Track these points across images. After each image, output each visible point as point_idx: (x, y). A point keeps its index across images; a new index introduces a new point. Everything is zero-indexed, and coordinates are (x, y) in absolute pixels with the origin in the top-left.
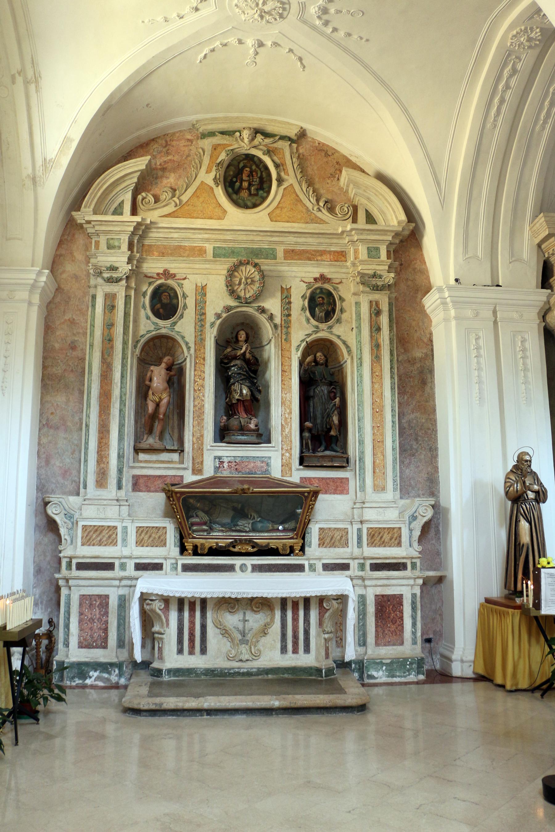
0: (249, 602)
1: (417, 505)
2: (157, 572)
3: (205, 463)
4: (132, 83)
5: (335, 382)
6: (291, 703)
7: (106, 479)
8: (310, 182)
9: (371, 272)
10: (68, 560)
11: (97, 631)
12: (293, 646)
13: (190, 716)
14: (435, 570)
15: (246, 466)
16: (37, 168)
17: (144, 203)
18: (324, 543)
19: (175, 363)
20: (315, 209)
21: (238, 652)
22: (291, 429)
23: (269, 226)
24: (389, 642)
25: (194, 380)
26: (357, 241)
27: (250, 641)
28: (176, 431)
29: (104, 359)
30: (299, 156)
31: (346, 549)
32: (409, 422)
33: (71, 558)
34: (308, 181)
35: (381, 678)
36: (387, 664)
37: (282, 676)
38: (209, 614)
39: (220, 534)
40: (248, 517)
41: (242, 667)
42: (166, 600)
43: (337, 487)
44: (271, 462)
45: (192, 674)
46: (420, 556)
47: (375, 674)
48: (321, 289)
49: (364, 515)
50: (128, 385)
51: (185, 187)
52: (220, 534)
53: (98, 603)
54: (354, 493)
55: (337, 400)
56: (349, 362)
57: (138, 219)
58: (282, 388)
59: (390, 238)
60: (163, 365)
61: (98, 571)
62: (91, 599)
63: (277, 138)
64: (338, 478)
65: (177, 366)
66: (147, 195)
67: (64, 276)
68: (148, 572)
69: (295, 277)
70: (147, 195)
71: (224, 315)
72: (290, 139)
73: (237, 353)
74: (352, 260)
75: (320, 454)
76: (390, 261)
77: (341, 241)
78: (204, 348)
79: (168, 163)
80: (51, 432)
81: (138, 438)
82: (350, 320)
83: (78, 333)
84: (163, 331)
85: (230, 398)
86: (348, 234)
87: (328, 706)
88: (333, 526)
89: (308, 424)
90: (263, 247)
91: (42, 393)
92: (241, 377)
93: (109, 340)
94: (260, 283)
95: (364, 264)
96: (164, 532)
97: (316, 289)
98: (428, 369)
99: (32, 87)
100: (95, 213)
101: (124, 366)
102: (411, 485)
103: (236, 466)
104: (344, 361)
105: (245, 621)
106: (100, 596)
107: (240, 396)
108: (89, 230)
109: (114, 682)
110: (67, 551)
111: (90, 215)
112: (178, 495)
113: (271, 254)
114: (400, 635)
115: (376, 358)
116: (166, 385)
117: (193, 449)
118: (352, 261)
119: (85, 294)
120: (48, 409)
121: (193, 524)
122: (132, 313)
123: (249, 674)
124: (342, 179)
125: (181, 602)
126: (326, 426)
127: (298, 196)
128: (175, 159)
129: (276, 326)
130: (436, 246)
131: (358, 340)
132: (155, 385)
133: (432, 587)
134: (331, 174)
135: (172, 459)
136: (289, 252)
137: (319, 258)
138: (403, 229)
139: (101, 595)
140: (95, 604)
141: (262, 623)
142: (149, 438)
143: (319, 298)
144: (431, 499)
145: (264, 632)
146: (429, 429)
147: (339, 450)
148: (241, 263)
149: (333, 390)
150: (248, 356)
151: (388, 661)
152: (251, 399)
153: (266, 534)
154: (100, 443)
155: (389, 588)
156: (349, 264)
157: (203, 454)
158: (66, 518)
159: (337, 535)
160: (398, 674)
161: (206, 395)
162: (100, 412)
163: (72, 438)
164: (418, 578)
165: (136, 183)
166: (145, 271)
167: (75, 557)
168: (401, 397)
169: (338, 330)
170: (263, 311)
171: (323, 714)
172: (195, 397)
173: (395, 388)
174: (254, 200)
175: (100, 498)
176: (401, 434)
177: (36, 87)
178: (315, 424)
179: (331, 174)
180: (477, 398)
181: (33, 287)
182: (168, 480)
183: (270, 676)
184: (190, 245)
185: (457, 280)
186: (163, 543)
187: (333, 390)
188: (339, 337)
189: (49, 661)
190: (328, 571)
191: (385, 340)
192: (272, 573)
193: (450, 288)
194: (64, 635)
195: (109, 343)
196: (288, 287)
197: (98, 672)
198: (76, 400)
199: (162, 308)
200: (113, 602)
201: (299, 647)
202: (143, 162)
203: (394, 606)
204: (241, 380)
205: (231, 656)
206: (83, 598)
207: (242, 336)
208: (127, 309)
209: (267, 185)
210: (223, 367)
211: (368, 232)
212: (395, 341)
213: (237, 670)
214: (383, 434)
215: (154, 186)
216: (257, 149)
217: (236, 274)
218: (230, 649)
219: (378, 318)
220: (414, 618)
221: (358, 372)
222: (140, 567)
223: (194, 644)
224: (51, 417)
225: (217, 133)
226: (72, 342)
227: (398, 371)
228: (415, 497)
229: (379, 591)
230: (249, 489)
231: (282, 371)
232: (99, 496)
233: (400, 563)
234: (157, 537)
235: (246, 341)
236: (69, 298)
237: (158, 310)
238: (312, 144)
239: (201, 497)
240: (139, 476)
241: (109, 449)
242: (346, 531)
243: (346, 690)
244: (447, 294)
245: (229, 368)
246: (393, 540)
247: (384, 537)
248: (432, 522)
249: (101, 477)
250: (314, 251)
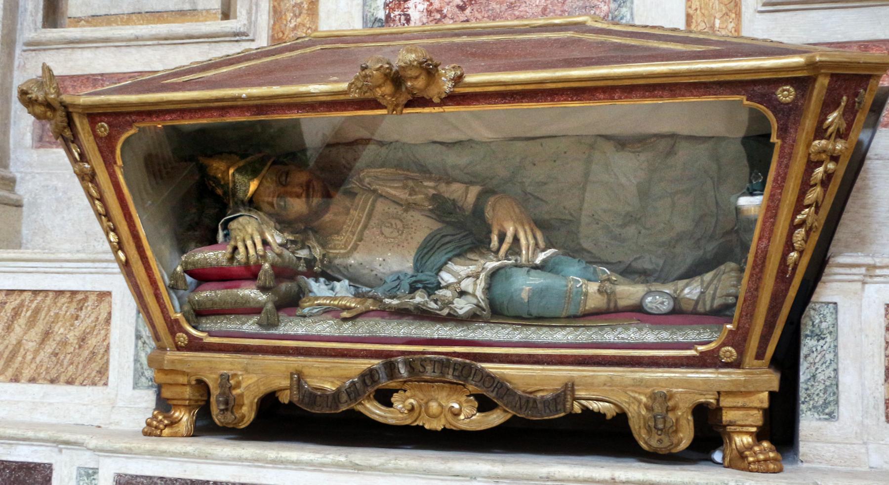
96: (104, 315)
234: (72, 337)
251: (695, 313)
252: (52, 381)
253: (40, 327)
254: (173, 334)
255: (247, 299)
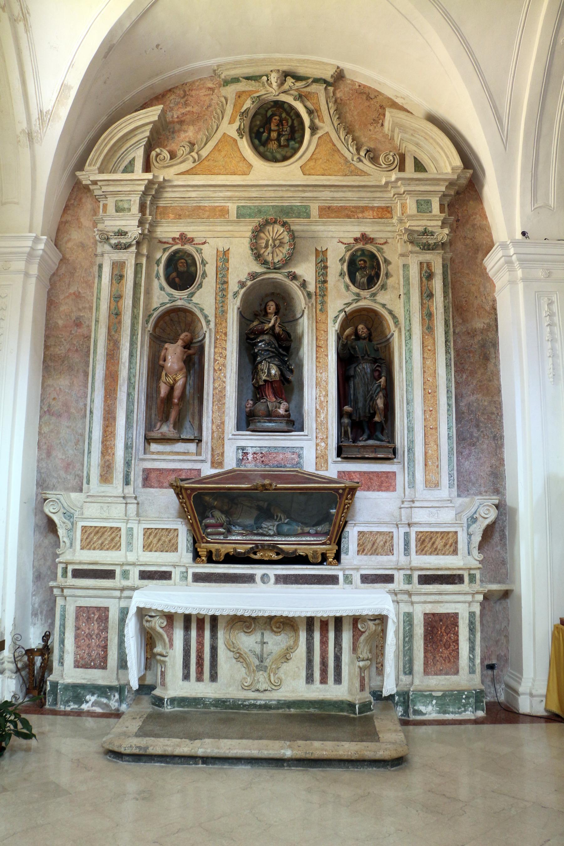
0: (268, 620)
1: (477, 504)
2: (164, 581)
3: (226, 454)
4: (134, 17)
5: (380, 359)
6: (306, 753)
7: (112, 473)
8: (349, 129)
9: (421, 229)
10: (64, 566)
11: (95, 648)
12: (321, 675)
13: (182, 763)
14: (499, 582)
15: (274, 458)
16: (33, 122)
17: (158, 160)
18: (364, 550)
19: (195, 341)
20: (355, 159)
21: (254, 680)
22: (327, 414)
23: (300, 179)
24: (441, 670)
25: (214, 359)
26: (404, 193)
27: (269, 668)
28: (197, 418)
29: (111, 336)
30: (336, 101)
31: (390, 557)
32: (469, 405)
33: (67, 564)
34: (347, 129)
35: (430, 714)
36: (437, 697)
37: (307, 710)
38: (221, 634)
39: (239, 538)
40: (273, 518)
41: (259, 698)
42: (170, 617)
43: (382, 482)
44: (303, 453)
45: (200, 705)
46: (480, 566)
47: (422, 708)
48: (363, 250)
49: (413, 516)
50: (138, 365)
51: (205, 140)
52: (239, 538)
53: (96, 617)
54: (403, 490)
55: (383, 380)
56: (396, 335)
57: (149, 176)
58: (317, 367)
59: (443, 189)
60: (180, 342)
61: (97, 580)
62: (88, 611)
63: (310, 81)
64: (384, 472)
65: (198, 344)
66: (161, 151)
67: (70, 245)
68: (155, 582)
69: (332, 237)
70: (161, 151)
71: (249, 283)
72: (325, 81)
73: (265, 326)
74: (399, 215)
75: (361, 444)
76: (443, 215)
77: (385, 195)
78: (226, 322)
79: (186, 115)
80: (54, 419)
81: (149, 427)
82: (397, 286)
83: (84, 308)
84: (179, 303)
85: (257, 379)
86: (394, 185)
87: (353, 758)
88: (375, 529)
89: (347, 408)
90: (295, 204)
91: (43, 376)
92: (269, 354)
93: (117, 314)
94: (291, 245)
95: (413, 220)
96: (176, 535)
97: (357, 251)
98: (491, 342)
99: (21, 26)
100: (101, 170)
101: (133, 343)
102: (471, 481)
103: (262, 457)
104: (391, 334)
105: (263, 643)
106: (98, 609)
107: (267, 376)
108: (97, 193)
109: (113, 708)
110: (66, 556)
111: (95, 174)
112: (189, 492)
113: (304, 212)
114: (454, 662)
115: (428, 329)
116: (182, 364)
117: (212, 439)
118: (398, 217)
119: (92, 264)
120: (49, 394)
121: (207, 526)
122: (143, 284)
123: (267, 707)
124: (386, 124)
125: (187, 618)
126: (369, 410)
127: (335, 145)
128: (194, 110)
129: (309, 295)
130: (498, 195)
131: (406, 308)
132: (169, 365)
133: (495, 603)
134: (374, 120)
135: (188, 450)
136: (325, 209)
137: (360, 215)
138: (459, 177)
139: (100, 607)
140: (94, 617)
141: (284, 646)
142: (163, 426)
143: (360, 260)
144: (494, 497)
145: (286, 657)
146: (493, 413)
147: (384, 438)
148: (267, 223)
149: (377, 368)
150: (277, 329)
151: (440, 694)
152: (280, 380)
153: (293, 539)
154: (105, 431)
155: (442, 605)
156: (395, 221)
157: (223, 445)
158: (65, 518)
159: (380, 540)
160: (451, 710)
161: (228, 376)
162: (105, 396)
163: (75, 427)
164: (477, 593)
165: (148, 137)
166: (159, 236)
167: (71, 563)
168: (458, 375)
169: (384, 297)
170: (294, 277)
171: (348, 768)
172: (216, 378)
173: (451, 365)
174: (284, 152)
175: (103, 494)
176: (459, 419)
177: (25, 25)
178: (355, 408)
179: (374, 120)
180: (551, 375)
181: (30, 256)
182: (184, 474)
183: (293, 711)
184: (210, 204)
185: (524, 234)
186: (174, 548)
187: (377, 368)
188: (384, 306)
189: (43, 681)
190: (368, 583)
191: (438, 308)
192: (299, 586)
193: (515, 243)
194: (60, 651)
195: (116, 318)
196: (323, 250)
197: (96, 696)
198: (81, 384)
199: (178, 277)
200: (114, 616)
201: (329, 676)
202: (154, 113)
203: (447, 626)
204: (270, 358)
205: (246, 684)
206: (80, 609)
207: (272, 307)
208: (137, 279)
209: (300, 135)
210: (249, 343)
211: (417, 182)
212: (451, 309)
213: (253, 702)
214: (436, 420)
215: (171, 142)
216: (288, 94)
217: (262, 235)
218: (245, 676)
219: (430, 283)
220: (472, 642)
221: (406, 346)
222: (145, 575)
223: (202, 669)
224: (53, 403)
225: (241, 79)
226: (77, 318)
227: (454, 345)
228: (476, 495)
229: (429, 608)
230: (271, 485)
231: (317, 346)
232: (103, 492)
233: (455, 575)
235: (276, 313)
236: (75, 269)
237: (174, 279)
238: (351, 86)
239: (218, 494)
240: (150, 469)
241: (115, 439)
242: (390, 535)
243: (380, 736)
244: (512, 251)
245: (256, 345)
246: (448, 547)
247: (437, 543)
248: (497, 525)
249: (106, 471)
250: (355, 207)
251: (320, 533)
252: (162, 551)
253: (158, 537)
254: (202, 540)
255: (220, 531)
